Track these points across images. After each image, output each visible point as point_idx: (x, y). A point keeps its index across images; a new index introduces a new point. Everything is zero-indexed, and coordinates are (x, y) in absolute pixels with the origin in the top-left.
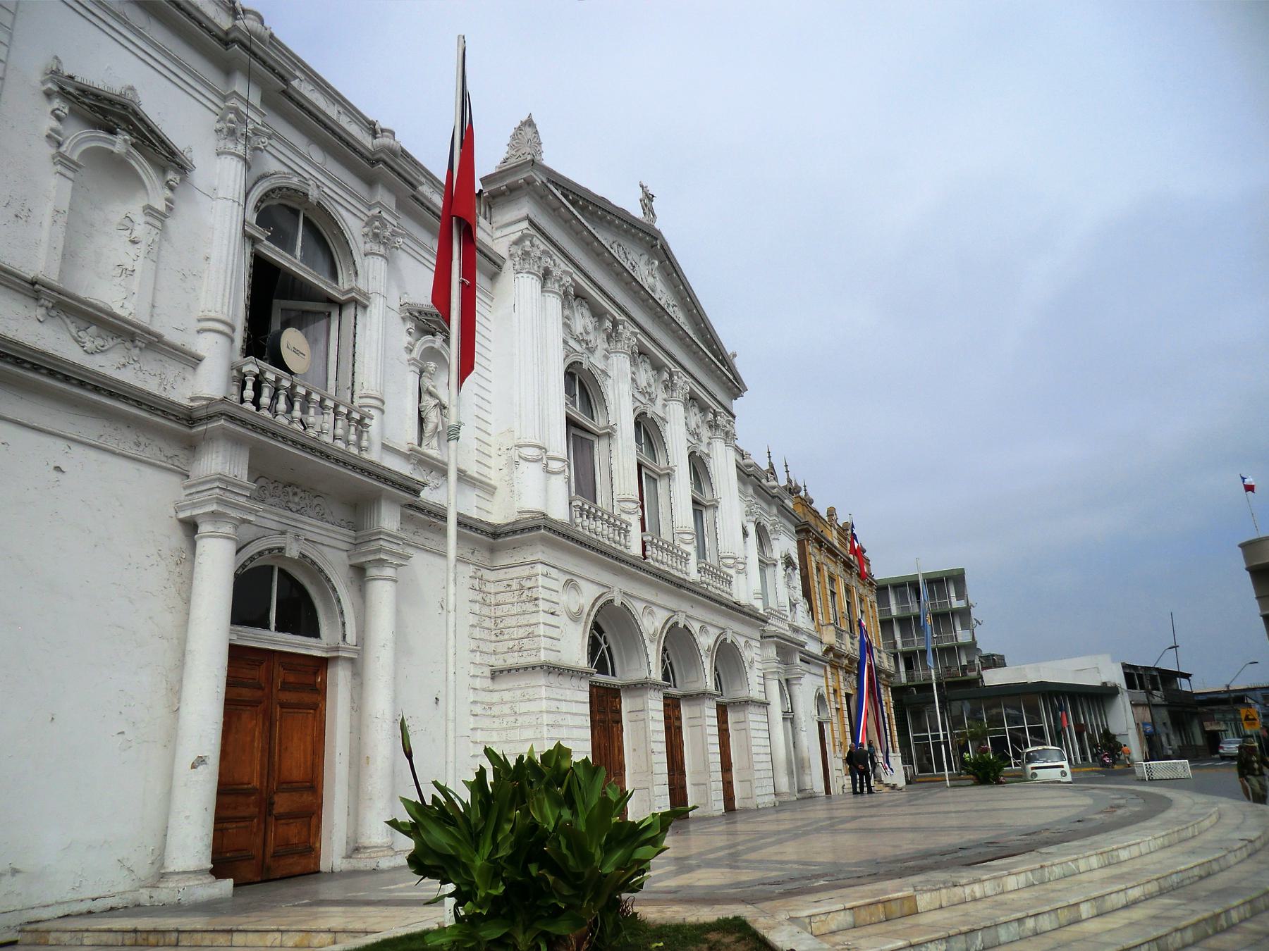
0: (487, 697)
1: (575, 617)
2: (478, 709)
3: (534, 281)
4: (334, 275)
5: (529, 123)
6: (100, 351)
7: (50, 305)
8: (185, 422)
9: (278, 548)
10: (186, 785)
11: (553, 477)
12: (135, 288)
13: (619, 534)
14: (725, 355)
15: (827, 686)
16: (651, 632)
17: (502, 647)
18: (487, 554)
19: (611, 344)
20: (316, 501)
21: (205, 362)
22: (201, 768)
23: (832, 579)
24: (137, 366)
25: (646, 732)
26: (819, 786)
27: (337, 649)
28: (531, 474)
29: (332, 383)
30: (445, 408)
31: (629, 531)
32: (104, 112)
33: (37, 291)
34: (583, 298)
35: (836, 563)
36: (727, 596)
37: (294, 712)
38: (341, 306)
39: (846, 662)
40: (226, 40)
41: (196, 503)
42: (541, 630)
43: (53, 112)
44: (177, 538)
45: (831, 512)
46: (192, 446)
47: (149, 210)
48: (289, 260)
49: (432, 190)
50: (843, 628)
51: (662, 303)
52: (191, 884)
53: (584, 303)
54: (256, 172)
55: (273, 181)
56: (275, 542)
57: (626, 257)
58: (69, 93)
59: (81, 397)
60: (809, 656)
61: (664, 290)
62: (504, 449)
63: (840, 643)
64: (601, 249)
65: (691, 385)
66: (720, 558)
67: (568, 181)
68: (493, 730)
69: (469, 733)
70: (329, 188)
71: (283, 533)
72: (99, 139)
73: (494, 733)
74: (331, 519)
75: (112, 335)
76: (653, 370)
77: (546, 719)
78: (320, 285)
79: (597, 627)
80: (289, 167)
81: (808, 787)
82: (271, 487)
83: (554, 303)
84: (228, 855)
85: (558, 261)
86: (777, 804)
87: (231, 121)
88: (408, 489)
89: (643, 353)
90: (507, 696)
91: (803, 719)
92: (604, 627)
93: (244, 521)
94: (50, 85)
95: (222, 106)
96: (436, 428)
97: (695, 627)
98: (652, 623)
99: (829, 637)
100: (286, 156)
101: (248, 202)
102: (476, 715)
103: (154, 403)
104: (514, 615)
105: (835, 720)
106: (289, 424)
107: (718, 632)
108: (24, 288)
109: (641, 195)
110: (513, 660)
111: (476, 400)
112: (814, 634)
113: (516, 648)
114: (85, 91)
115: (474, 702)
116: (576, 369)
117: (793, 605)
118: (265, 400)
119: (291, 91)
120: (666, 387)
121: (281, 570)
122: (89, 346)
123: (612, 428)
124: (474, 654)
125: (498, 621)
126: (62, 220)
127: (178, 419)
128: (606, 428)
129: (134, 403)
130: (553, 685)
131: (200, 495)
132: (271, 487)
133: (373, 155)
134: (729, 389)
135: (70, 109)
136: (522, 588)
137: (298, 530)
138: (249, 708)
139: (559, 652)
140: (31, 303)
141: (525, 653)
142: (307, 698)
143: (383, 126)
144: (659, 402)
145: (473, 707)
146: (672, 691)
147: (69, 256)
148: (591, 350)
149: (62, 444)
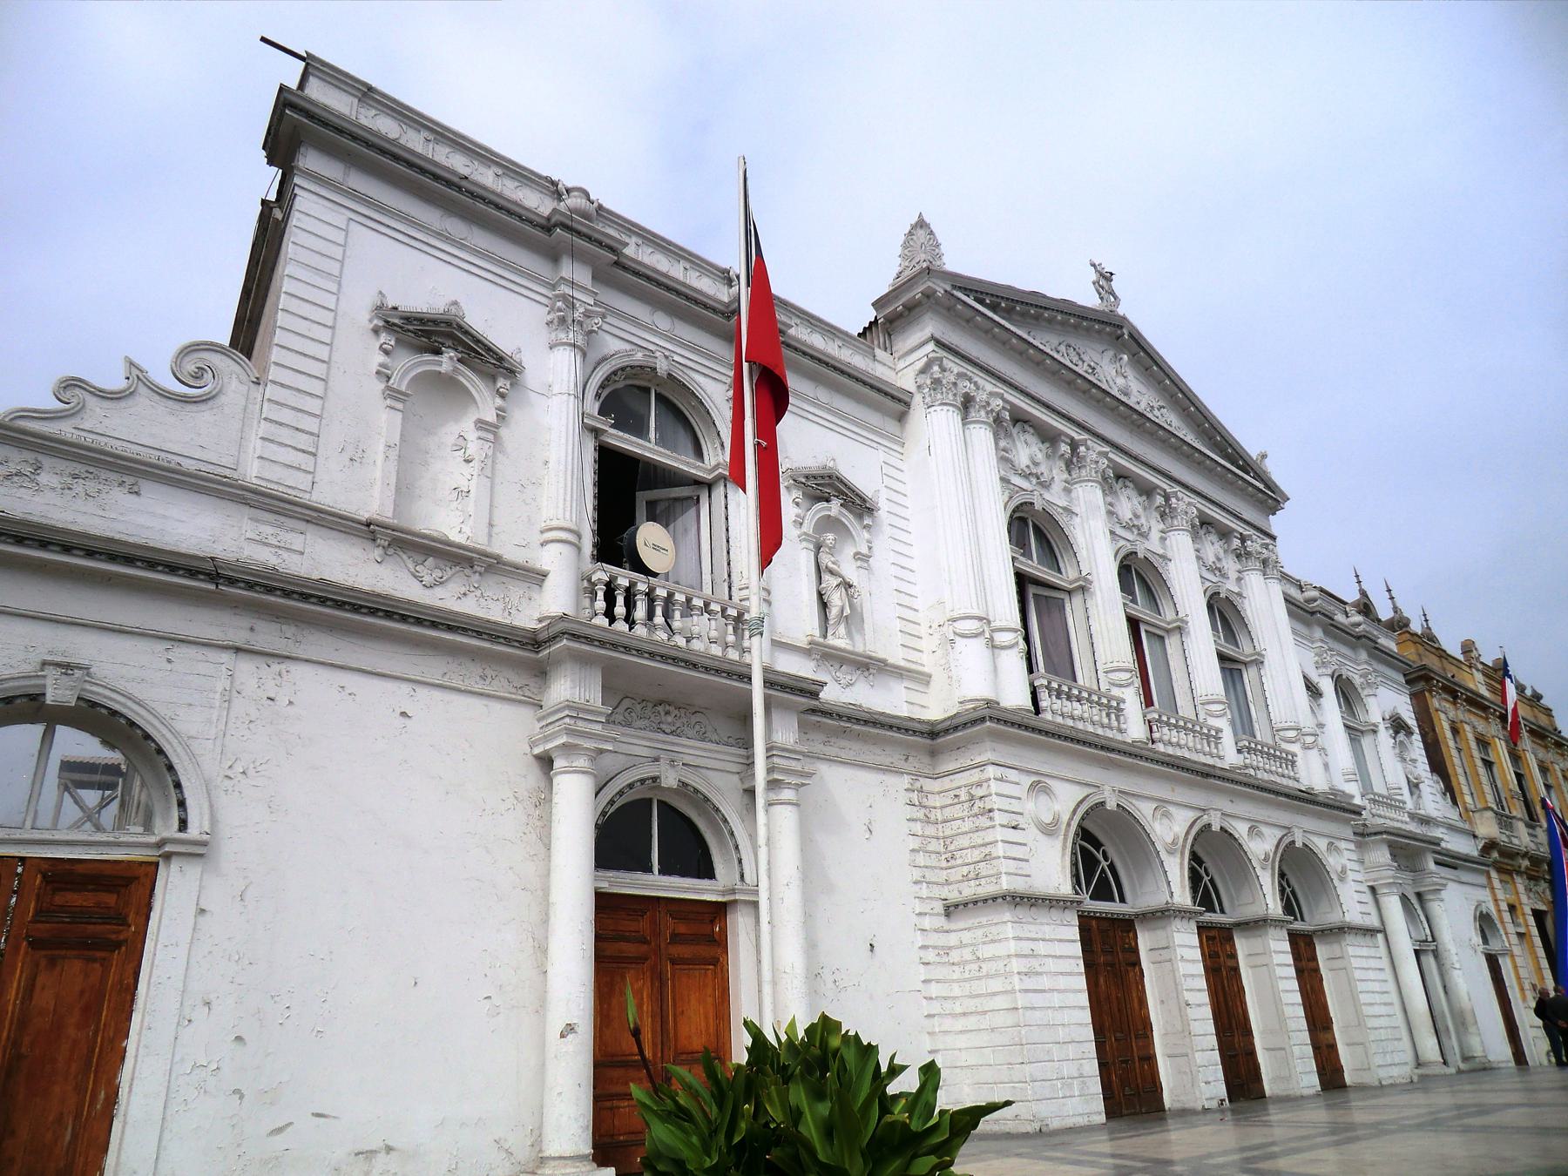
0: (940, 940)
1: (1048, 830)
2: (930, 956)
3: (951, 413)
4: (699, 453)
5: (921, 224)
6: (440, 583)
7: (387, 543)
8: (530, 647)
9: (652, 778)
10: (556, 1057)
11: (1004, 653)
12: (471, 510)
13: (1108, 715)
14: (1247, 458)
15: (1496, 900)
16: (1169, 840)
17: (956, 874)
18: (926, 760)
19: (1073, 473)
20: (694, 719)
21: (550, 577)
22: (570, 1037)
23: (1483, 743)
24: (478, 593)
25: (1174, 976)
26: (1501, 1051)
27: (733, 891)
28: (972, 653)
29: (707, 577)
30: (850, 586)
31: (1122, 710)
32: (427, 334)
33: (373, 532)
34: (1025, 422)
35: (1487, 719)
36: (1291, 783)
37: (689, 969)
38: (709, 486)
39: (1525, 863)
40: (547, 226)
41: (549, 735)
42: (1000, 850)
43: (381, 346)
44: (534, 774)
45: (1468, 648)
46: (542, 673)
47: (481, 425)
48: (642, 445)
49: (809, 330)
50: (1514, 813)
51: (1140, 408)
52: (568, 1171)
53: (1027, 427)
54: (594, 356)
55: (613, 363)
56: (647, 771)
57: (1081, 359)
58: (394, 324)
59: (390, 629)
60: (1453, 857)
61: (1143, 390)
62: (935, 626)
63: (1508, 836)
64: (1040, 357)
65: (1199, 505)
66: (1275, 731)
67: (980, 281)
68: (953, 981)
69: (920, 986)
70: (681, 355)
71: (657, 759)
72: (426, 363)
73: (955, 986)
74: (715, 737)
75: (449, 564)
76: (1141, 495)
77: (1016, 965)
78: (681, 467)
79: (1195, 857)
80: (632, 343)
81: (1478, 1052)
82: (639, 707)
83: (982, 436)
84: (622, 1138)
85: (981, 382)
86: (1415, 1079)
87: (560, 310)
88: (802, 692)
89: (1206, 523)
90: (967, 937)
91: (1453, 951)
92: (1205, 858)
93: (601, 751)
94: (375, 322)
95: (550, 296)
96: (842, 611)
97: (1240, 829)
98: (1260, 847)
99: (1488, 827)
100: (507, 279)
101: (586, 391)
102: (928, 963)
103: (495, 630)
104: (966, 833)
105: (1517, 950)
106: (741, 656)
107: (1279, 833)
108: (361, 531)
109: (1094, 277)
110: (969, 891)
111: (894, 570)
112: (1460, 825)
113: (972, 875)
114: (408, 319)
115: (924, 947)
116: (1027, 512)
117: (1414, 786)
118: (620, 609)
119: (625, 261)
120: (1163, 515)
121: (661, 804)
122: (427, 579)
123: (1085, 579)
124: (919, 886)
125: (949, 841)
126: (394, 454)
127: (522, 645)
128: (1254, 655)
129: (474, 634)
130: (1024, 920)
131: (550, 727)
132: (639, 707)
133: (727, 307)
134: (1261, 503)
135: (398, 341)
136: (972, 798)
137: (673, 754)
138: (634, 966)
139: (1029, 876)
140: (369, 545)
141: (983, 881)
142: (704, 951)
143: (569, 185)
144: (1155, 535)
145: (922, 953)
146: (1298, 926)
147: (404, 489)
148: (1045, 485)
149: (406, 688)
